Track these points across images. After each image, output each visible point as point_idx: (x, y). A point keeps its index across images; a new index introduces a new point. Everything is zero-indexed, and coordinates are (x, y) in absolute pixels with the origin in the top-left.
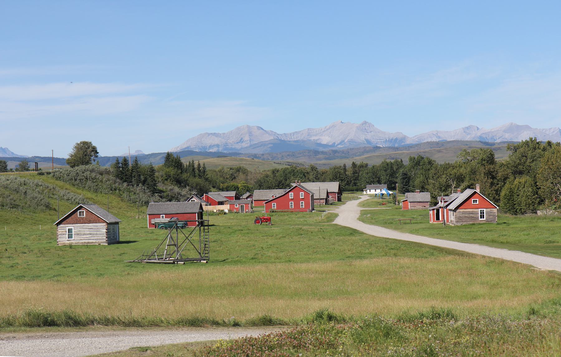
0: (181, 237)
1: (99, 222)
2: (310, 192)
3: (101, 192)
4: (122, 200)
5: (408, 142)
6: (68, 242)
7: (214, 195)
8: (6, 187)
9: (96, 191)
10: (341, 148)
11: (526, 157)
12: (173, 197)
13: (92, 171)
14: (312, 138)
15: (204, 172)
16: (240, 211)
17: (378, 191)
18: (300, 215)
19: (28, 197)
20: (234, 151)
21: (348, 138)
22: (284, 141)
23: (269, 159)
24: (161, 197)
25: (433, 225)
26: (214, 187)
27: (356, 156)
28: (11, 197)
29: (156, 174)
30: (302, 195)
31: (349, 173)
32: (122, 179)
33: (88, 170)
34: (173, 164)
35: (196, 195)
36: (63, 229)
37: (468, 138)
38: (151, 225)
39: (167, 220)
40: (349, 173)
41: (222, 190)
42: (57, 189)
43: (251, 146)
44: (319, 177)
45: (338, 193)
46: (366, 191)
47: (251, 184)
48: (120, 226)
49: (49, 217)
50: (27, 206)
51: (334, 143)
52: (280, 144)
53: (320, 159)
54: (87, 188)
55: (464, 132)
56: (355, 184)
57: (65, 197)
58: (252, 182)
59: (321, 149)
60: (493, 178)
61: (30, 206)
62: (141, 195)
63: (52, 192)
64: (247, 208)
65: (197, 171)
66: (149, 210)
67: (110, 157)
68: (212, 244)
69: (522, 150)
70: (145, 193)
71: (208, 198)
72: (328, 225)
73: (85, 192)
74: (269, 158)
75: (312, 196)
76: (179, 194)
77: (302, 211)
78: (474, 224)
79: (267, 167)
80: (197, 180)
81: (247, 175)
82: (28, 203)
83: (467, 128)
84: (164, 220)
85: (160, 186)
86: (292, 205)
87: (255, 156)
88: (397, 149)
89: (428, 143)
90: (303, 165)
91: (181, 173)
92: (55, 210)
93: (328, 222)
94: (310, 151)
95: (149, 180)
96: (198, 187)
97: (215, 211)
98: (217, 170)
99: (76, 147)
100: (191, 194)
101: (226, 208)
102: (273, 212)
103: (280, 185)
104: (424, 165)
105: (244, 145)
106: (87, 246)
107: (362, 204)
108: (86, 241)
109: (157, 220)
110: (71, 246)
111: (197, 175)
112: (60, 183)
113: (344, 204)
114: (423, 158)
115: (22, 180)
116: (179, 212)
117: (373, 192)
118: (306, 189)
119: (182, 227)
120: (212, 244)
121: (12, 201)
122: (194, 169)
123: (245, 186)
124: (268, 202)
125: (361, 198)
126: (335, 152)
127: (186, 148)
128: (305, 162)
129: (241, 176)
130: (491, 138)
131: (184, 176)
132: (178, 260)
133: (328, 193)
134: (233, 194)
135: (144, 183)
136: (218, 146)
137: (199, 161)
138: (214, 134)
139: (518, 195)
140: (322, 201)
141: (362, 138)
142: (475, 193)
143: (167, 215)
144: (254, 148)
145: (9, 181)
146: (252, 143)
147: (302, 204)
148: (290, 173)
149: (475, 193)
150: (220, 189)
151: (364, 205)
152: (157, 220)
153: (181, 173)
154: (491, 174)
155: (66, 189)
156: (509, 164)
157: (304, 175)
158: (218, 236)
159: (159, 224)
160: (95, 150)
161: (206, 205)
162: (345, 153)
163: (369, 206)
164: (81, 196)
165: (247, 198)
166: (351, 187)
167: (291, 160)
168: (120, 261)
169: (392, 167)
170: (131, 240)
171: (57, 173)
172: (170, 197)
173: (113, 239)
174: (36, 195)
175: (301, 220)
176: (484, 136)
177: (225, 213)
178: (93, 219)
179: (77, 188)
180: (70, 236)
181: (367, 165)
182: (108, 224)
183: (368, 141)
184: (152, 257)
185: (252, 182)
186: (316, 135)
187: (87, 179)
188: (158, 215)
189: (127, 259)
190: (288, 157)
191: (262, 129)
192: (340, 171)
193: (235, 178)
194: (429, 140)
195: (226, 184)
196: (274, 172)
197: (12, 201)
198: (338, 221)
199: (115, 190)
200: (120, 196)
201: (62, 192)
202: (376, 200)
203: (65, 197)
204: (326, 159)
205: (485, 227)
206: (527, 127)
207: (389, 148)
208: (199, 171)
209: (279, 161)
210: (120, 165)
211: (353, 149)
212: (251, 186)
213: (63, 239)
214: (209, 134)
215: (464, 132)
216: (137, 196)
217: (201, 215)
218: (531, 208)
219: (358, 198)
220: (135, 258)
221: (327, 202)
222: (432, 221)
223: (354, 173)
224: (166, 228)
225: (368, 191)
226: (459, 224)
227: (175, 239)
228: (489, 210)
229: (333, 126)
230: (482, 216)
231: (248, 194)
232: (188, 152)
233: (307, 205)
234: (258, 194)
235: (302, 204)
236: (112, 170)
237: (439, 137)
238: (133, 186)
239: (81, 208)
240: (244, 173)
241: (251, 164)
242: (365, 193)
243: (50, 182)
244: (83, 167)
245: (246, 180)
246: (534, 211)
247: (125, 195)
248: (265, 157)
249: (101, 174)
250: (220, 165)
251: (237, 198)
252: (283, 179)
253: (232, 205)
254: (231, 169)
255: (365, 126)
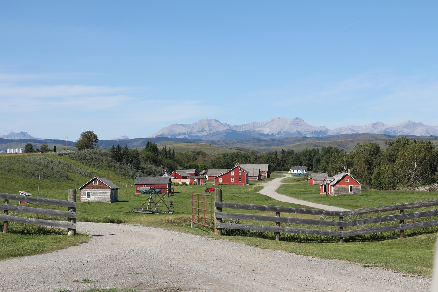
0: (158, 198)
1: (106, 189)
2: (246, 171)
3: (102, 168)
4: (116, 174)
5: (330, 134)
6: (87, 200)
7: (180, 172)
8: (39, 164)
9: (98, 167)
10: (278, 137)
11: (398, 150)
12: (152, 173)
13: (96, 153)
14: (257, 129)
15: (174, 155)
16: (197, 183)
17: (300, 172)
18: (238, 187)
19: (55, 171)
20: (197, 138)
21: (284, 130)
22: (235, 131)
23: (223, 145)
24: (143, 173)
25: (322, 195)
26: (180, 166)
27: (289, 144)
28: (44, 170)
29: (140, 156)
30: (240, 173)
31: (279, 157)
32: (116, 159)
33: (92, 153)
34: (152, 149)
35: (167, 172)
36: (84, 192)
37: (375, 132)
38: (137, 190)
39: (148, 188)
40: (279, 157)
41: (186, 168)
42: (73, 165)
43: (210, 134)
44: (257, 160)
45: (268, 172)
46: (291, 171)
47: (208, 164)
48: (119, 191)
49: (69, 185)
50: (54, 177)
51: (273, 133)
52: (232, 134)
53: (261, 146)
54: (92, 165)
55: (373, 127)
56: (283, 165)
57: (78, 172)
58: (209, 162)
59: (263, 138)
60: (370, 164)
61: (56, 177)
62: (130, 171)
63: (70, 168)
64: (202, 181)
65: (168, 154)
66: (136, 181)
67: (103, 141)
68: (175, 204)
69: (395, 145)
70: (132, 169)
71: (175, 174)
72: (253, 194)
73: (90, 168)
74: (224, 144)
75: (247, 174)
76: (155, 170)
77: (240, 184)
78: (345, 195)
79: (218, 152)
80: (168, 161)
81: (205, 157)
82: (55, 175)
83: (375, 124)
84: (145, 188)
85: (142, 165)
86: (233, 180)
87: (213, 142)
88: (321, 139)
89: (344, 135)
90: (249, 150)
91: (157, 156)
92: (72, 180)
93: (255, 192)
94: (254, 139)
95: (135, 160)
96: (169, 166)
97: (180, 183)
98: (183, 153)
99: (82, 135)
100: (164, 171)
101: (187, 181)
102: (220, 184)
103: (229, 165)
104: (333, 153)
105: (205, 133)
106: (99, 203)
107: (284, 181)
108: (98, 200)
109: (141, 188)
110: (89, 203)
111: (168, 157)
112: (75, 161)
113: (272, 180)
114: (332, 148)
115: (50, 159)
116: (155, 183)
117: (295, 172)
118: (243, 169)
119: (158, 193)
120: (175, 204)
121: (44, 174)
122: (166, 153)
123: (203, 166)
124: (217, 178)
125: (285, 176)
126: (274, 140)
127: (160, 135)
128: (250, 147)
129: (201, 158)
130: (394, 132)
131: (160, 158)
132: (155, 212)
133: (260, 172)
134: (193, 171)
135: (131, 162)
136: (185, 134)
137: (169, 146)
138: (182, 125)
139: (384, 177)
140: (255, 178)
141: (294, 130)
142: (347, 175)
143: (148, 185)
144: (212, 136)
145: (41, 160)
146: (211, 132)
147: (240, 180)
148: (236, 156)
149: (347, 175)
150: (185, 167)
151: (285, 181)
152: (141, 188)
153: (157, 156)
154: (368, 162)
155: (78, 166)
156: (386, 154)
157: (246, 158)
158: (181, 199)
159: (142, 191)
160: (95, 137)
161: (174, 179)
162: (281, 142)
163: (288, 182)
164: (89, 171)
165: (203, 174)
166: (280, 168)
167: (239, 146)
168: (121, 212)
169: (310, 154)
170: (125, 200)
171: (72, 155)
172: (149, 173)
173: (115, 199)
174: (60, 170)
175: (237, 190)
176: (388, 130)
177: (187, 185)
178: (102, 186)
179: (86, 165)
180: (88, 197)
181: (293, 152)
182: (112, 190)
183: (299, 132)
184: (140, 210)
185: (209, 162)
186: (259, 127)
187: (92, 159)
188: (142, 185)
189: (125, 211)
190: (238, 143)
191: (219, 122)
192: (272, 156)
193: (196, 159)
194: (346, 133)
195: (189, 164)
196: (225, 155)
197: (44, 174)
198: (262, 192)
199: (111, 167)
200: (115, 171)
201: (76, 168)
202: (296, 178)
203: (78, 172)
204: (266, 145)
205: (352, 197)
206: (421, 124)
207: (315, 138)
208: (170, 154)
209: (230, 147)
210: (115, 149)
211: (287, 138)
212: (207, 165)
213: (84, 199)
214: (178, 125)
215: (373, 127)
216: (126, 172)
217: (170, 185)
218: (392, 185)
219: (283, 176)
220: (130, 210)
221: (259, 179)
222: (322, 193)
223: (283, 158)
224: (147, 193)
225: (292, 171)
226: (336, 195)
227: (154, 199)
228: (356, 186)
229: (273, 121)
230: (351, 190)
231: (204, 171)
232: (162, 138)
233: (243, 180)
234: (211, 172)
235: (240, 180)
236: (109, 153)
237: (354, 131)
238: (124, 164)
239: (95, 179)
240: (203, 156)
241: (209, 149)
242: (290, 172)
243: (68, 161)
244: (89, 150)
245: (204, 161)
246: (394, 188)
247: (118, 171)
248: (220, 143)
249: (102, 156)
250: (186, 149)
251: (196, 174)
252: (229, 161)
253: (192, 180)
254: (193, 152)
255: (297, 121)
